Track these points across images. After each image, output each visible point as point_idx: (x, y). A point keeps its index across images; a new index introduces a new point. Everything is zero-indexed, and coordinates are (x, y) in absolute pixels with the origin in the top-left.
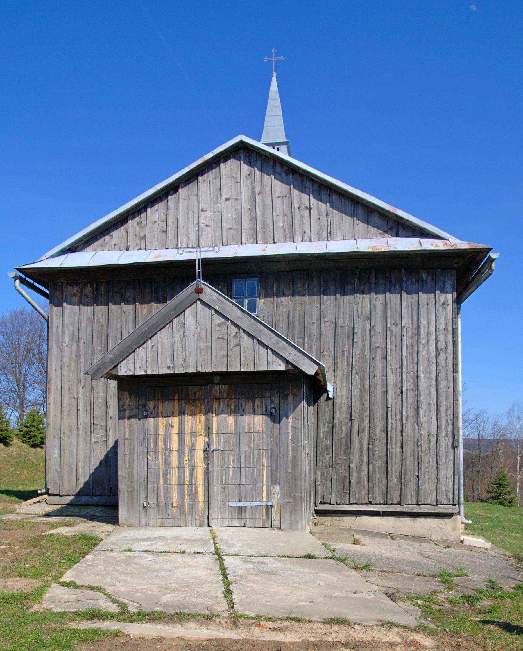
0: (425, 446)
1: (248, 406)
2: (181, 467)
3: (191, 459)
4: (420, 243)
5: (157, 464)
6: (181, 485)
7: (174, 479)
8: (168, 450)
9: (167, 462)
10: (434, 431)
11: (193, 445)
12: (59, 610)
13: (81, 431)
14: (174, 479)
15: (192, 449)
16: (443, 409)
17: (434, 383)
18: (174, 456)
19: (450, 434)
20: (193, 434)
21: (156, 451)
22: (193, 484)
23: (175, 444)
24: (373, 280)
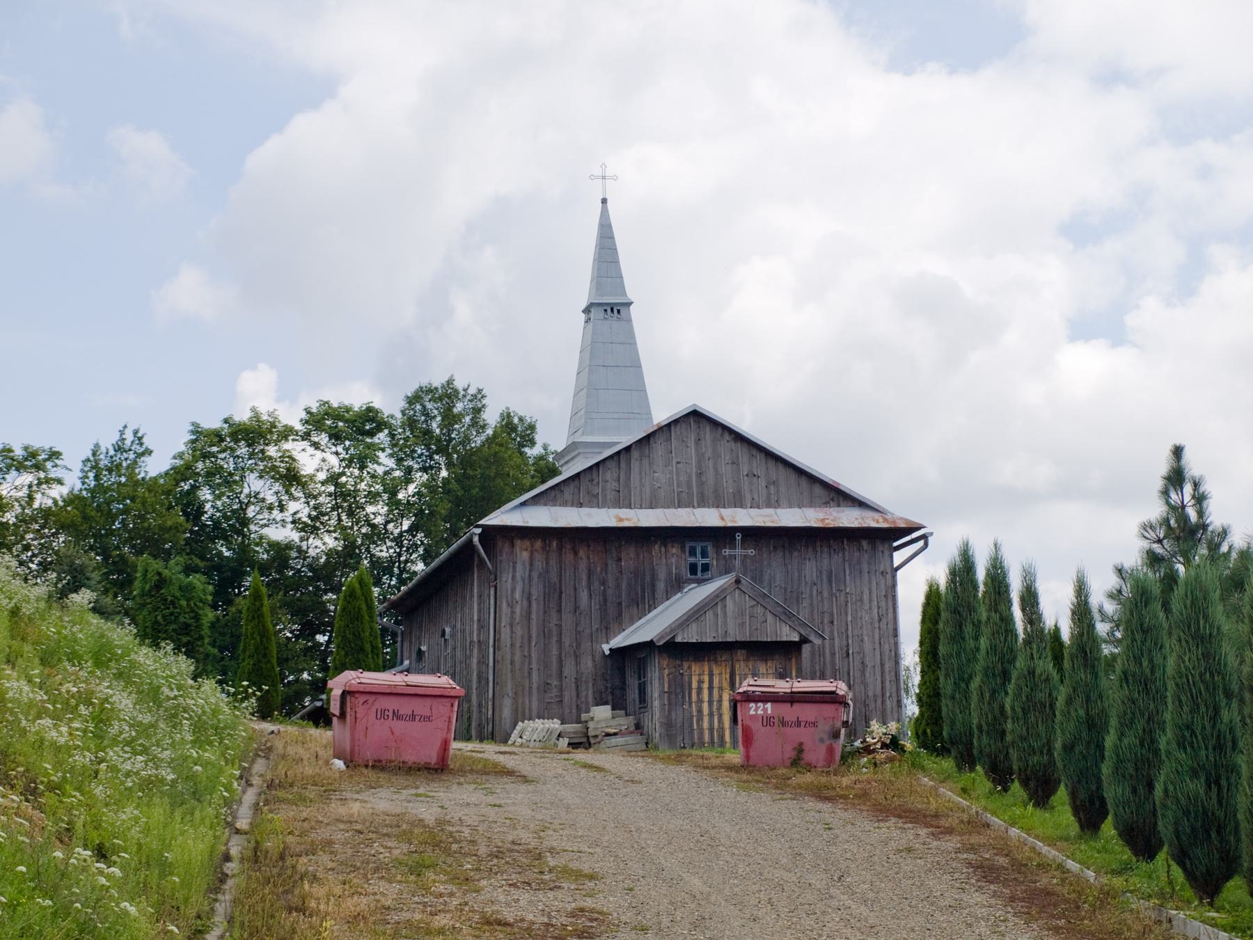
0: (872, 706)
1: (762, 668)
2: (711, 715)
3: (720, 708)
4: (722, 519)
5: (691, 713)
6: (711, 729)
7: (706, 725)
8: (700, 701)
9: (700, 711)
10: (879, 692)
11: (721, 697)
12: (1162, 746)
13: (535, 691)
14: (706, 725)
15: (720, 701)
16: (887, 670)
17: (877, 646)
18: (705, 706)
19: (894, 695)
20: (721, 689)
21: (690, 703)
22: (721, 729)
23: (706, 697)
24: (865, 567)
